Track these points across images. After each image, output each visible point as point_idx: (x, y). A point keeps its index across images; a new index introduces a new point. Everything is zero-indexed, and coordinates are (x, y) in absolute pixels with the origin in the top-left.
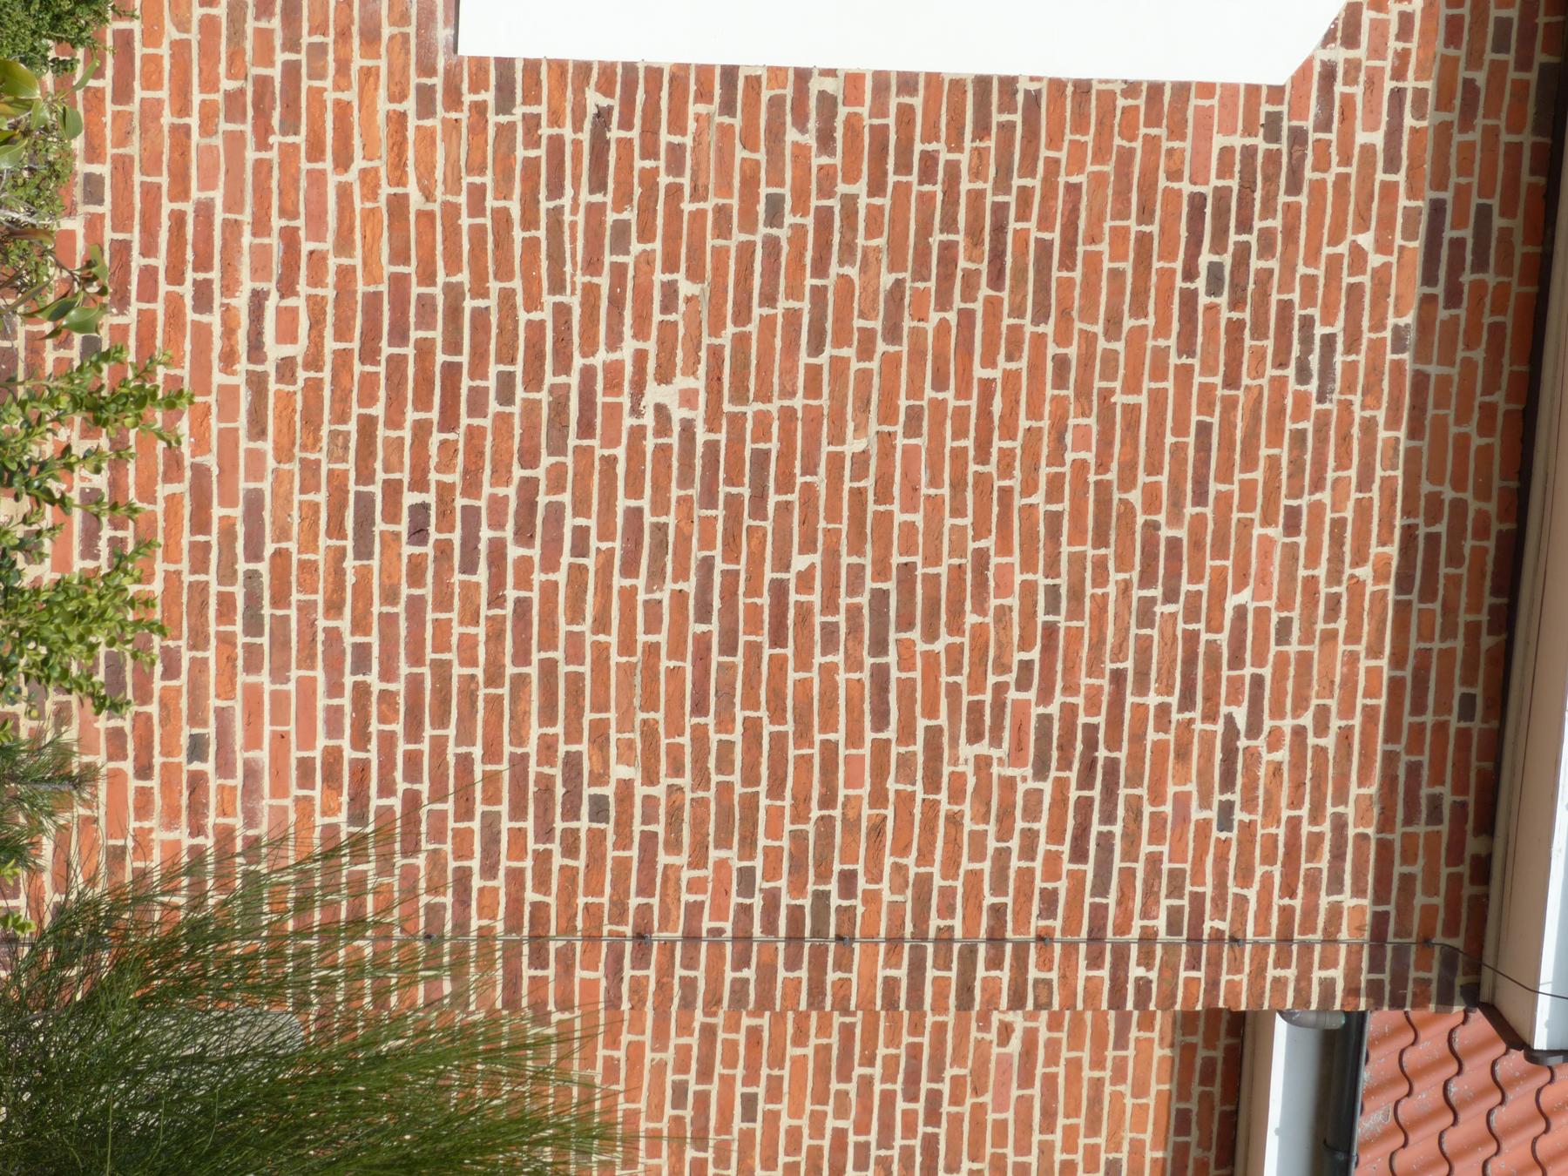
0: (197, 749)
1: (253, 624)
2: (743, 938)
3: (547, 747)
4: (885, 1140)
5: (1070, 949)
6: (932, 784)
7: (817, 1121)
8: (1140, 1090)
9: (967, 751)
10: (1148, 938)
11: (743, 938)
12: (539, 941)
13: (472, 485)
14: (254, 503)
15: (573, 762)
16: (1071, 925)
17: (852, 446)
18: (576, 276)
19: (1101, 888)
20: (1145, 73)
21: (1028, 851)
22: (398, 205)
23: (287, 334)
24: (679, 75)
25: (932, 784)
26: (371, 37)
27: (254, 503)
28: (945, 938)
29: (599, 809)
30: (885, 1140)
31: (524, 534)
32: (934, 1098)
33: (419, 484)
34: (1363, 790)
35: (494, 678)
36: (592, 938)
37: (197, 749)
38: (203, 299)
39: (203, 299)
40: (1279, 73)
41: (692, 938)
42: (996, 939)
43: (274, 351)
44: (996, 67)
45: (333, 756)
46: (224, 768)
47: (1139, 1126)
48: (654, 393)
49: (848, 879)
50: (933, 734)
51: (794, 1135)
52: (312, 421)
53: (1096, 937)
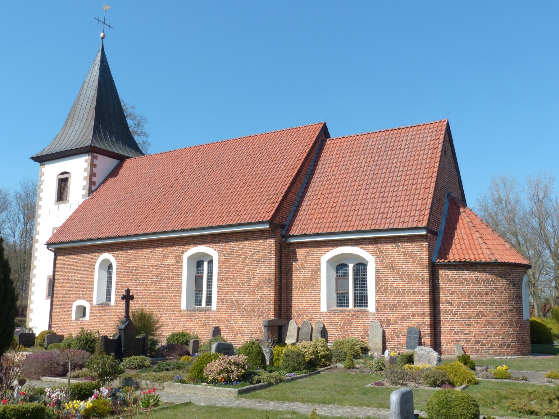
0: (256, 328)
1: (249, 324)
2: (270, 287)
3: (257, 302)
4: (302, 272)
5: (422, 247)
6: (259, 273)
7: (301, 277)
8: (400, 246)
9: (258, 271)
10: (270, 256)
11: (270, 287)
12: (269, 302)
13: (241, 308)
14: (242, 324)
15: (258, 300)
16: (420, 247)
17: (239, 281)
18: (229, 301)
19: (266, 260)
20: (217, 263)
21: (264, 266)
22: (225, 314)
23: (232, 321)
24: (218, 295)
25: (259, 273)
26: (215, 316)
27: (242, 324)
28: (270, 271)
29: (261, 298)
30: (302, 272)
31: (244, 304)
32: (300, 268)
33: (405, 267)
34: (261, 241)
35: (390, 269)
36: (269, 298)
37: (256, 328)
38: (230, 327)
39: (230, 327)
40: (217, 253)
41: (269, 291)
42: (270, 267)
43: (233, 322)
44: (217, 273)
45: (257, 318)
46: (258, 326)
47: (403, 246)
48: (235, 296)
49: (266, 279)
50: (257, 274)
51: (302, 279)
52: (237, 319)
53: (270, 260)
